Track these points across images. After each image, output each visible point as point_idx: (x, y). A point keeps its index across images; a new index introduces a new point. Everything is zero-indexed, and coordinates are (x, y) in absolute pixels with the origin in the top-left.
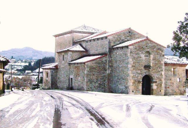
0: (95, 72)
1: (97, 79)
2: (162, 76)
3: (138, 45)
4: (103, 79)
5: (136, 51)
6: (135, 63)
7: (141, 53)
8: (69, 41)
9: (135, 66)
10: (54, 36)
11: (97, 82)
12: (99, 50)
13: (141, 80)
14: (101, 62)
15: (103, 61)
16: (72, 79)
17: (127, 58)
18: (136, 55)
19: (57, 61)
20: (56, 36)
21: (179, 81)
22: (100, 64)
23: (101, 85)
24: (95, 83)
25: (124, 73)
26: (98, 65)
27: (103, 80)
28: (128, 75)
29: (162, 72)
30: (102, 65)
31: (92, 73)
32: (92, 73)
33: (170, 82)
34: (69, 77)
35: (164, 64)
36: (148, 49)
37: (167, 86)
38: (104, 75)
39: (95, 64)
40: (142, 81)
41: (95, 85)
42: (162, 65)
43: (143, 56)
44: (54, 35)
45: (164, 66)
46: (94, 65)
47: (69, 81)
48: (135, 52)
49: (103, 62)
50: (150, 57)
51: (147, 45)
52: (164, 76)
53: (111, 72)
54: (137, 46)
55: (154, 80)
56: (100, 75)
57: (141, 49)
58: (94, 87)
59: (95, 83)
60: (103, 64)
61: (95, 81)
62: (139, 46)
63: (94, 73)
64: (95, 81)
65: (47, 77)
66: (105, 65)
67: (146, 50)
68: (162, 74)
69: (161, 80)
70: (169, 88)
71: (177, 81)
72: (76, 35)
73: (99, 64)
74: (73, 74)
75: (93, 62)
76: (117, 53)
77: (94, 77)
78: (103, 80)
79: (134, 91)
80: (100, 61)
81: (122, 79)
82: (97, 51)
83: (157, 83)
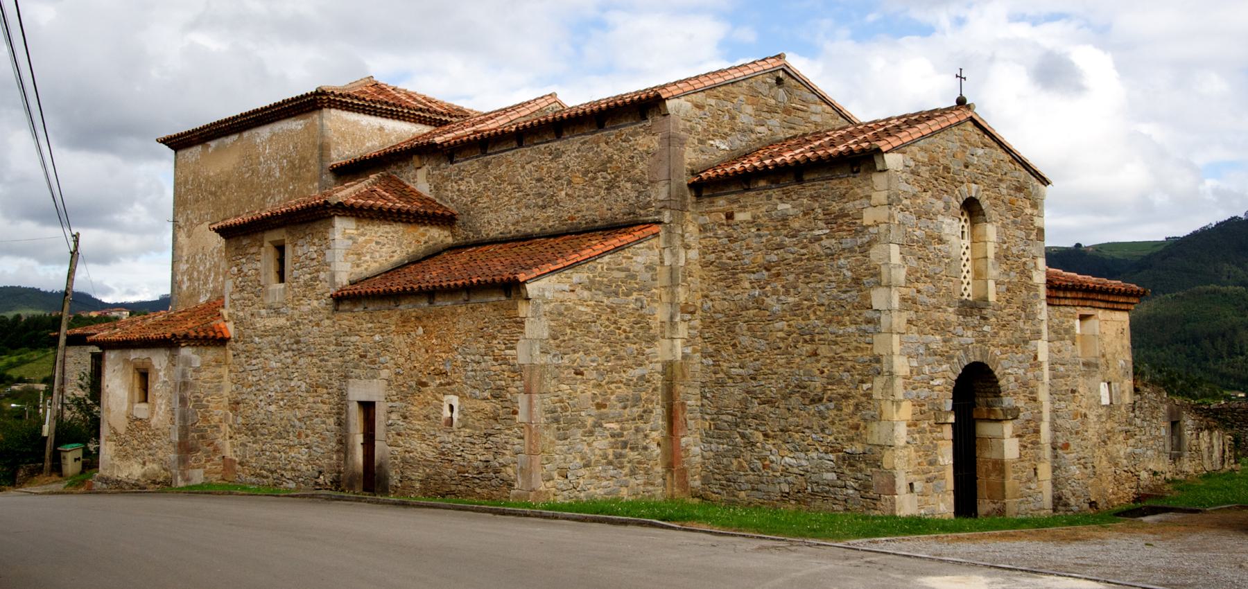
3: (926, 151)
4: (637, 400)
7: (939, 205)
8: (291, 162)
11: (598, 424)
12: (569, 205)
13: (949, 405)
14: (623, 275)
16: (368, 408)
17: (848, 242)
18: (919, 218)
20: (178, 143)
22: (617, 294)
24: (591, 433)
25: (824, 350)
27: (637, 411)
28: (876, 366)
31: (566, 361)
32: (566, 361)
34: (343, 396)
35: (1043, 292)
36: (974, 186)
37: (1061, 441)
38: (638, 372)
39: (586, 294)
40: (954, 406)
41: (589, 445)
42: (1037, 296)
44: (164, 135)
45: (1044, 304)
46: (583, 301)
47: (342, 424)
49: (633, 277)
52: (1046, 374)
53: (689, 350)
55: (1008, 402)
58: (585, 466)
59: (591, 433)
60: (635, 295)
62: (932, 161)
64: (590, 422)
65: (145, 400)
67: (964, 188)
68: (1040, 359)
69: (1035, 400)
72: (346, 122)
74: (385, 373)
75: (576, 277)
76: (740, 217)
77: (585, 392)
80: (617, 274)
81: (795, 400)
82: (550, 211)
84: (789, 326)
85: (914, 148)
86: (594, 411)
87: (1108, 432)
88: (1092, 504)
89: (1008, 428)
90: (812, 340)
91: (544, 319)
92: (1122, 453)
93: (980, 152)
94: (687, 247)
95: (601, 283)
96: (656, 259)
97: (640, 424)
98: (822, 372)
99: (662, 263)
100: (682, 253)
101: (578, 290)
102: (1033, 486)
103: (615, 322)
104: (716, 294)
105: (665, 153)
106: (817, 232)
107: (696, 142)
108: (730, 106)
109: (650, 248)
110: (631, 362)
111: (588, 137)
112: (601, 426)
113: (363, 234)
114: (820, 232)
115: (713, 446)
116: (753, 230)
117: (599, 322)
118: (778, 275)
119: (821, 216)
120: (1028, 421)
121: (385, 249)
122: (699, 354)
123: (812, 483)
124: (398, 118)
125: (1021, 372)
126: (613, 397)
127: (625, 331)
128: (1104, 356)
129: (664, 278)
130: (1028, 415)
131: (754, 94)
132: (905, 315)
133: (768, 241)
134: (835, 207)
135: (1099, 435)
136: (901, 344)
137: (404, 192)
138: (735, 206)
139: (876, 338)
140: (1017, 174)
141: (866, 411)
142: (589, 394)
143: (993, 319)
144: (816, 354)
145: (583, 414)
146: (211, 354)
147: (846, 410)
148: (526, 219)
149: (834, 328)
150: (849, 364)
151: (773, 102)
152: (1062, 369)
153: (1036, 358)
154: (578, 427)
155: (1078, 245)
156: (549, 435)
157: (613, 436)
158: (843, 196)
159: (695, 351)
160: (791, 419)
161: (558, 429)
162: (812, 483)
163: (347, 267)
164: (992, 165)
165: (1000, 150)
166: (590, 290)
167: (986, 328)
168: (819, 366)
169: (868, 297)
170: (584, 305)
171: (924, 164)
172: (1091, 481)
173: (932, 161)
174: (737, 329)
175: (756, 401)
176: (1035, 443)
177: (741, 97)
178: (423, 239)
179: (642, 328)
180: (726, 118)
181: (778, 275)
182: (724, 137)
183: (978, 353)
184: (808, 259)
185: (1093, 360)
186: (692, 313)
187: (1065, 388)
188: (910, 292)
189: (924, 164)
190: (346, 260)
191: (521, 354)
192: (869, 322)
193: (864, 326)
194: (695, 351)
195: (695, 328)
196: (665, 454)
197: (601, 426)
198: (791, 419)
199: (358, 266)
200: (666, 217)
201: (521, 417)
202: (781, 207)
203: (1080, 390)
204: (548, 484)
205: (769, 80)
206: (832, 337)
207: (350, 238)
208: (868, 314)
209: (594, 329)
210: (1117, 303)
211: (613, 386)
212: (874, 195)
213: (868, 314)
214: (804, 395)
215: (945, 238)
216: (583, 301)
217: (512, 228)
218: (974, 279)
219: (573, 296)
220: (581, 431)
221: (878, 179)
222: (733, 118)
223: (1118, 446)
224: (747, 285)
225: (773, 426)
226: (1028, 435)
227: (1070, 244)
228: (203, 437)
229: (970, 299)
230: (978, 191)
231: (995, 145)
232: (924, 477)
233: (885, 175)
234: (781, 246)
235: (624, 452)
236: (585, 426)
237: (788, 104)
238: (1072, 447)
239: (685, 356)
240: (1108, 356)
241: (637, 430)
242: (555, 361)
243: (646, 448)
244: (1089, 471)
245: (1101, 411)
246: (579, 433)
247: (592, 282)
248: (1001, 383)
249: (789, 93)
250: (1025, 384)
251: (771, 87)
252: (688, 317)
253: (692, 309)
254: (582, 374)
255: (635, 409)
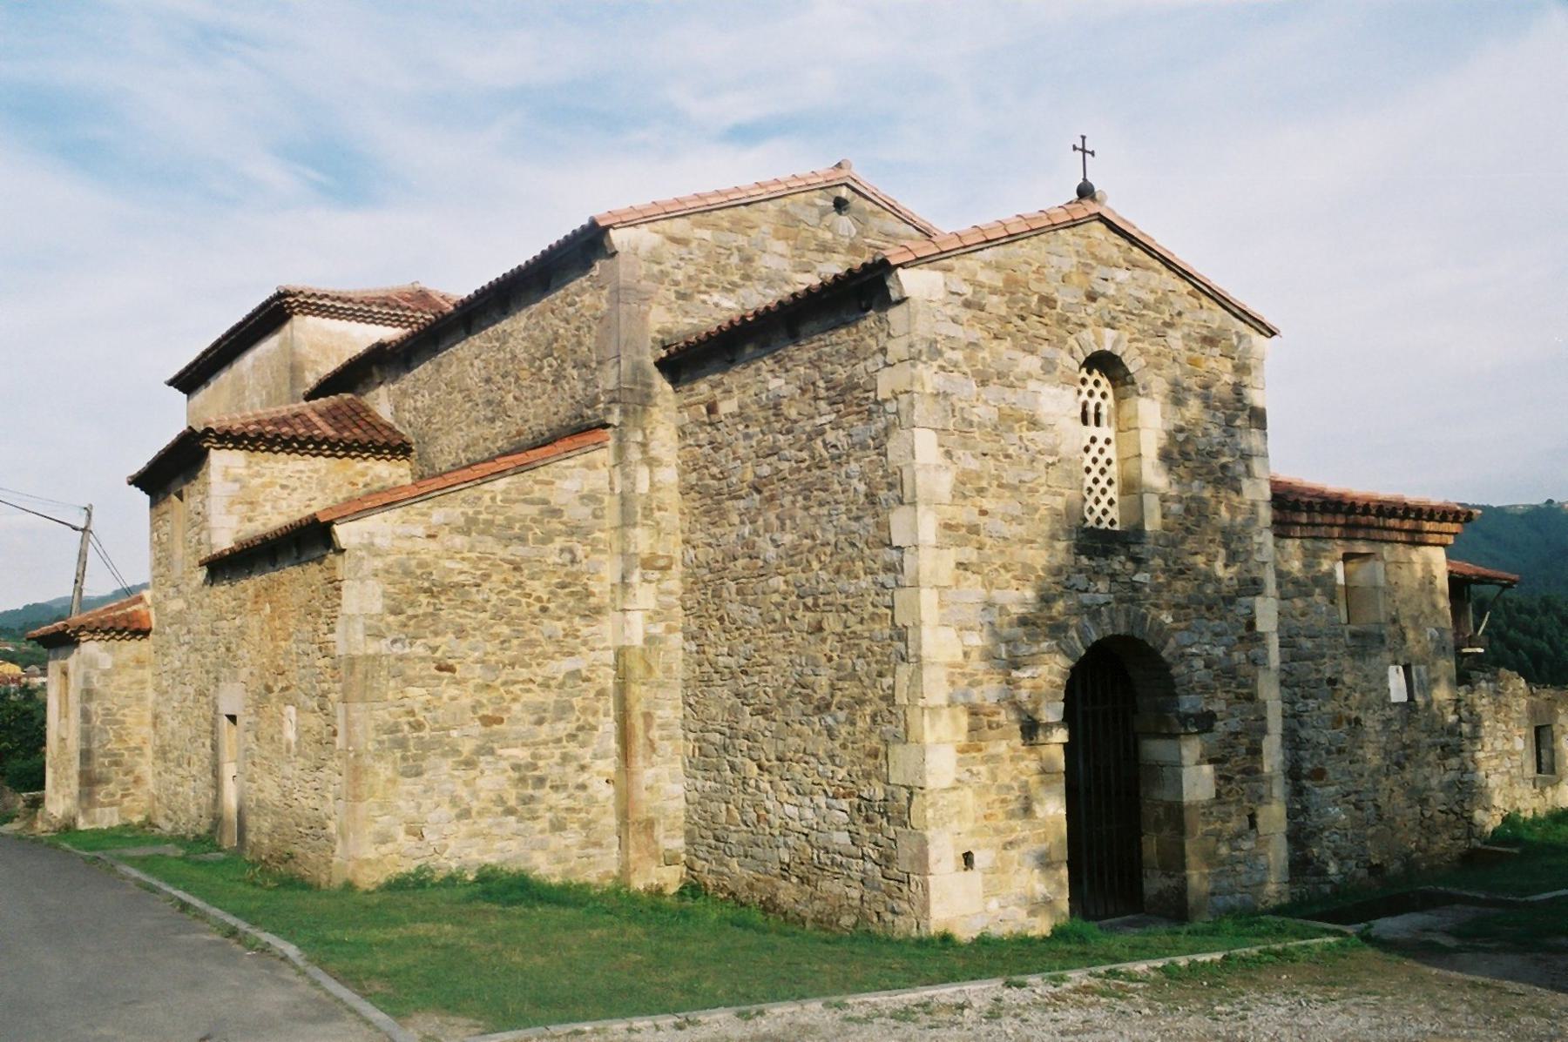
0: (461, 633)
1: (487, 721)
2: (1256, 651)
3: (998, 267)
4: (563, 710)
5: (977, 334)
6: (981, 491)
7: (1031, 363)
9: (974, 529)
10: (171, 383)
14: (533, 511)
15: (556, 500)
19: (1236, 849)
21: (1405, 699)
22: (522, 539)
23: (540, 781)
24: (469, 764)
25: (832, 623)
26: (501, 552)
27: (563, 728)
29: (1259, 601)
30: (552, 554)
31: (419, 649)
33: (1328, 708)
35: (1266, 514)
36: (1109, 334)
37: (1307, 766)
38: (567, 665)
39: (459, 540)
43: (1058, 404)
46: (452, 553)
48: (973, 345)
49: (556, 513)
50: (1126, 428)
51: (1099, 287)
53: (658, 629)
54: (983, 276)
55: (1189, 703)
56: (525, 673)
57: (1033, 326)
58: (459, 817)
60: (559, 542)
61: (468, 737)
62: (1011, 287)
63: (446, 642)
64: (467, 748)
66: (580, 551)
67: (1087, 335)
68: (1261, 627)
69: (1251, 698)
70: (1318, 774)
71: (1384, 700)
72: (329, 333)
73: (511, 534)
76: (727, 407)
78: (563, 728)
79: (977, 857)
83: (1219, 726)
84: (786, 582)
85: (973, 262)
86: (476, 728)
87: (1405, 747)
88: (1375, 870)
89: (1191, 749)
90: (816, 605)
91: (371, 582)
92: (1434, 782)
93: (1122, 275)
94: (651, 462)
95: (490, 523)
96: (603, 484)
97: (572, 748)
98: (830, 659)
99: (612, 489)
100: (643, 475)
101: (444, 534)
102: (1247, 845)
103: (520, 585)
104: (699, 537)
105: (614, 315)
106: (819, 421)
107: (673, 297)
108: (741, 240)
109: (591, 466)
110: (550, 649)
111: (535, 307)
112: (491, 752)
113: (259, 475)
114: (823, 420)
115: (699, 784)
116: (741, 427)
117: (486, 586)
118: (772, 498)
119: (823, 393)
120: (1236, 735)
121: (296, 495)
122: (680, 635)
123: (819, 848)
124: (364, 320)
125: (1219, 651)
126: (516, 707)
127: (539, 599)
128: (1394, 621)
129: (612, 516)
130: (1235, 724)
131: (789, 225)
132: (953, 555)
133: (759, 443)
134: (841, 374)
135: (1387, 753)
136: (941, 605)
137: (361, 415)
138: (718, 392)
139: (900, 595)
140: (1204, 315)
141: (890, 722)
142: (466, 701)
143: (1157, 562)
144: (820, 629)
145: (454, 733)
146: (131, 648)
147: (860, 724)
148: (475, 442)
149: (843, 582)
150: (865, 644)
151: (829, 236)
152: (1309, 644)
153: (1251, 625)
154: (444, 755)
155: (1550, 502)
156: (384, 770)
157: (516, 767)
158: (852, 354)
159: (670, 630)
160: (790, 740)
161: (404, 759)
162: (819, 848)
163: (233, 522)
164: (1151, 298)
165: (1166, 274)
166: (468, 533)
167: (1140, 577)
168: (826, 648)
169: (884, 526)
170: (453, 558)
171: (994, 291)
172: (1370, 831)
173: (1011, 287)
174: (725, 594)
175: (748, 710)
176: (1252, 772)
177: (764, 228)
178: (361, 481)
179: (572, 594)
180: (735, 259)
181: (772, 498)
182: (731, 288)
183: (1121, 621)
184: (809, 469)
185: (1373, 629)
186: (663, 569)
187: (1314, 676)
188: (965, 514)
189: (994, 291)
190: (229, 512)
191: (350, 640)
192: (889, 568)
193: (882, 577)
194: (670, 630)
195: (671, 593)
196: (618, 793)
197: (491, 752)
198: (790, 740)
199: (250, 520)
200: (615, 418)
201: (339, 741)
202: (774, 384)
203: (1347, 679)
204: (384, 849)
205: (820, 202)
206: (841, 599)
207: (236, 480)
208: (890, 556)
209: (478, 598)
210: (1385, 528)
211: (516, 688)
212: (890, 345)
213: (890, 556)
214: (806, 699)
215: (1045, 420)
216: (452, 553)
217: (462, 456)
218: (1122, 494)
219: (433, 545)
220: (450, 761)
221: (894, 314)
222: (748, 260)
223: (1427, 771)
224: (736, 519)
225: (769, 751)
226: (1239, 765)
227: (1539, 500)
228: (116, 763)
229: (1117, 527)
230: (1117, 342)
231: (1157, 264)
232: (997, 840)
233: (903, 307)
234: (774, 451)
235: (537, 793)
236: (457, 752)
237: (859, 240)
238: (1331, 775)
239: (649, 640)
240: (1406, 623)
241: (565, 758)
242: (398, 649)
243: (583, 787)
244: (1370, 811)
245: (1388, 712)
246: (447, 765)
247: (471, 522)
248: (1174, 671)
249: (861, 220)
250: (1230, 672)
251: (823, 213)
252: (657, 575)
253: (661, 563)
254: (451, 669)
255: (560, 725)
